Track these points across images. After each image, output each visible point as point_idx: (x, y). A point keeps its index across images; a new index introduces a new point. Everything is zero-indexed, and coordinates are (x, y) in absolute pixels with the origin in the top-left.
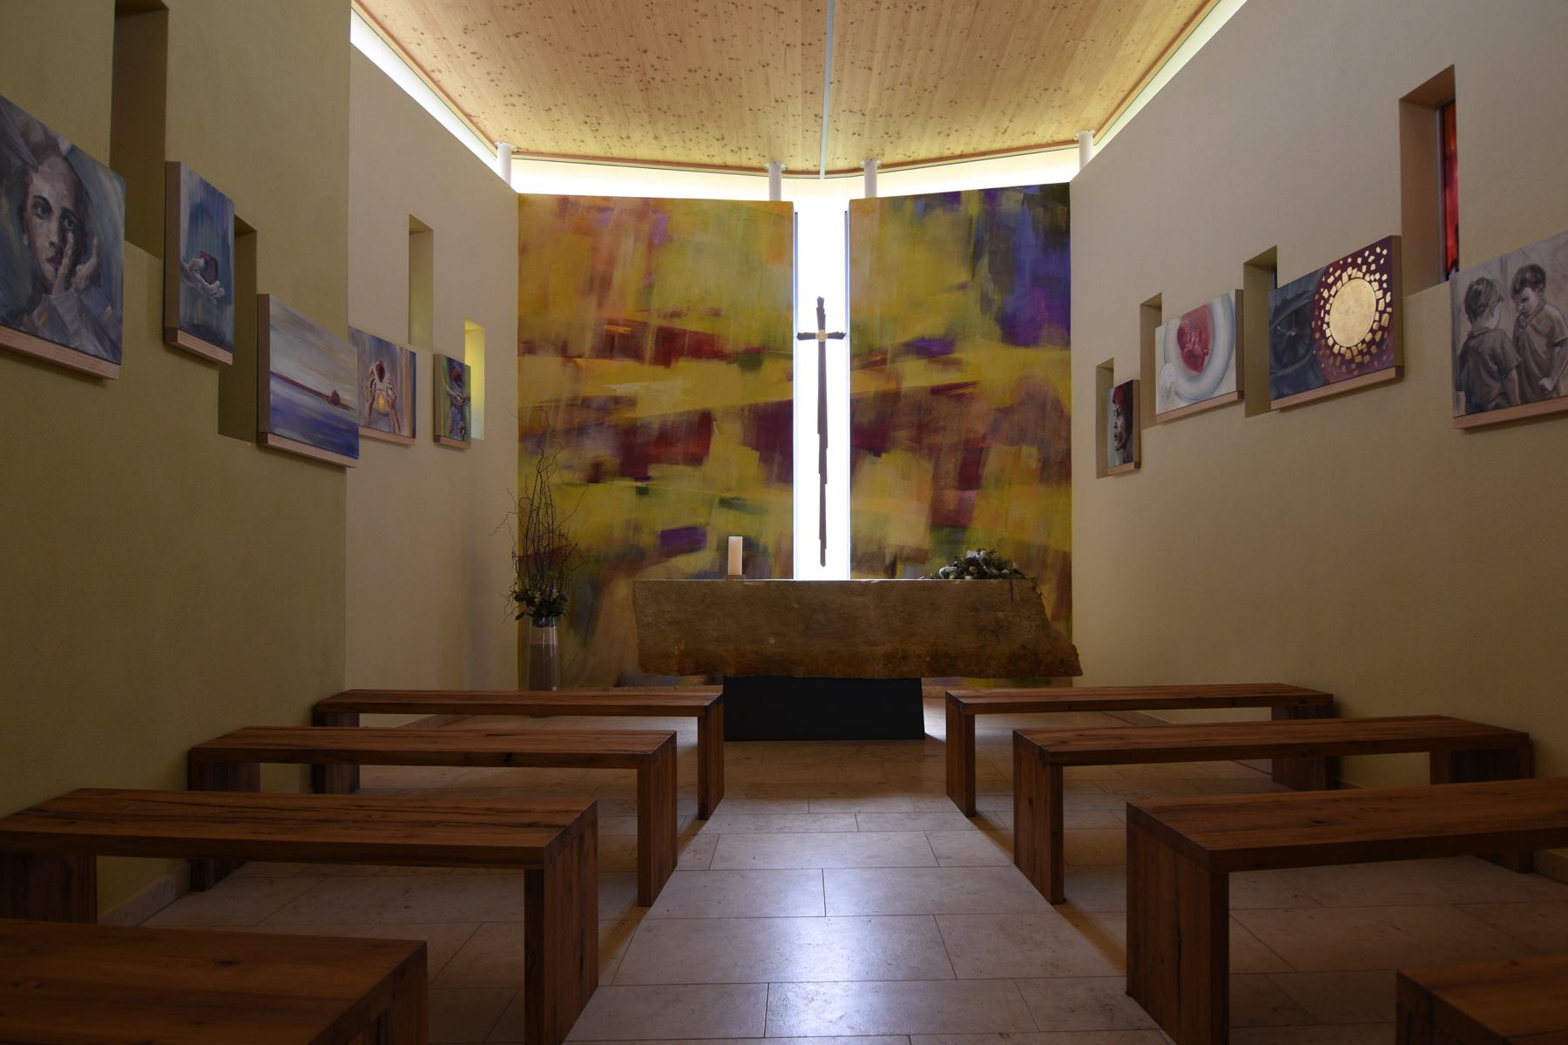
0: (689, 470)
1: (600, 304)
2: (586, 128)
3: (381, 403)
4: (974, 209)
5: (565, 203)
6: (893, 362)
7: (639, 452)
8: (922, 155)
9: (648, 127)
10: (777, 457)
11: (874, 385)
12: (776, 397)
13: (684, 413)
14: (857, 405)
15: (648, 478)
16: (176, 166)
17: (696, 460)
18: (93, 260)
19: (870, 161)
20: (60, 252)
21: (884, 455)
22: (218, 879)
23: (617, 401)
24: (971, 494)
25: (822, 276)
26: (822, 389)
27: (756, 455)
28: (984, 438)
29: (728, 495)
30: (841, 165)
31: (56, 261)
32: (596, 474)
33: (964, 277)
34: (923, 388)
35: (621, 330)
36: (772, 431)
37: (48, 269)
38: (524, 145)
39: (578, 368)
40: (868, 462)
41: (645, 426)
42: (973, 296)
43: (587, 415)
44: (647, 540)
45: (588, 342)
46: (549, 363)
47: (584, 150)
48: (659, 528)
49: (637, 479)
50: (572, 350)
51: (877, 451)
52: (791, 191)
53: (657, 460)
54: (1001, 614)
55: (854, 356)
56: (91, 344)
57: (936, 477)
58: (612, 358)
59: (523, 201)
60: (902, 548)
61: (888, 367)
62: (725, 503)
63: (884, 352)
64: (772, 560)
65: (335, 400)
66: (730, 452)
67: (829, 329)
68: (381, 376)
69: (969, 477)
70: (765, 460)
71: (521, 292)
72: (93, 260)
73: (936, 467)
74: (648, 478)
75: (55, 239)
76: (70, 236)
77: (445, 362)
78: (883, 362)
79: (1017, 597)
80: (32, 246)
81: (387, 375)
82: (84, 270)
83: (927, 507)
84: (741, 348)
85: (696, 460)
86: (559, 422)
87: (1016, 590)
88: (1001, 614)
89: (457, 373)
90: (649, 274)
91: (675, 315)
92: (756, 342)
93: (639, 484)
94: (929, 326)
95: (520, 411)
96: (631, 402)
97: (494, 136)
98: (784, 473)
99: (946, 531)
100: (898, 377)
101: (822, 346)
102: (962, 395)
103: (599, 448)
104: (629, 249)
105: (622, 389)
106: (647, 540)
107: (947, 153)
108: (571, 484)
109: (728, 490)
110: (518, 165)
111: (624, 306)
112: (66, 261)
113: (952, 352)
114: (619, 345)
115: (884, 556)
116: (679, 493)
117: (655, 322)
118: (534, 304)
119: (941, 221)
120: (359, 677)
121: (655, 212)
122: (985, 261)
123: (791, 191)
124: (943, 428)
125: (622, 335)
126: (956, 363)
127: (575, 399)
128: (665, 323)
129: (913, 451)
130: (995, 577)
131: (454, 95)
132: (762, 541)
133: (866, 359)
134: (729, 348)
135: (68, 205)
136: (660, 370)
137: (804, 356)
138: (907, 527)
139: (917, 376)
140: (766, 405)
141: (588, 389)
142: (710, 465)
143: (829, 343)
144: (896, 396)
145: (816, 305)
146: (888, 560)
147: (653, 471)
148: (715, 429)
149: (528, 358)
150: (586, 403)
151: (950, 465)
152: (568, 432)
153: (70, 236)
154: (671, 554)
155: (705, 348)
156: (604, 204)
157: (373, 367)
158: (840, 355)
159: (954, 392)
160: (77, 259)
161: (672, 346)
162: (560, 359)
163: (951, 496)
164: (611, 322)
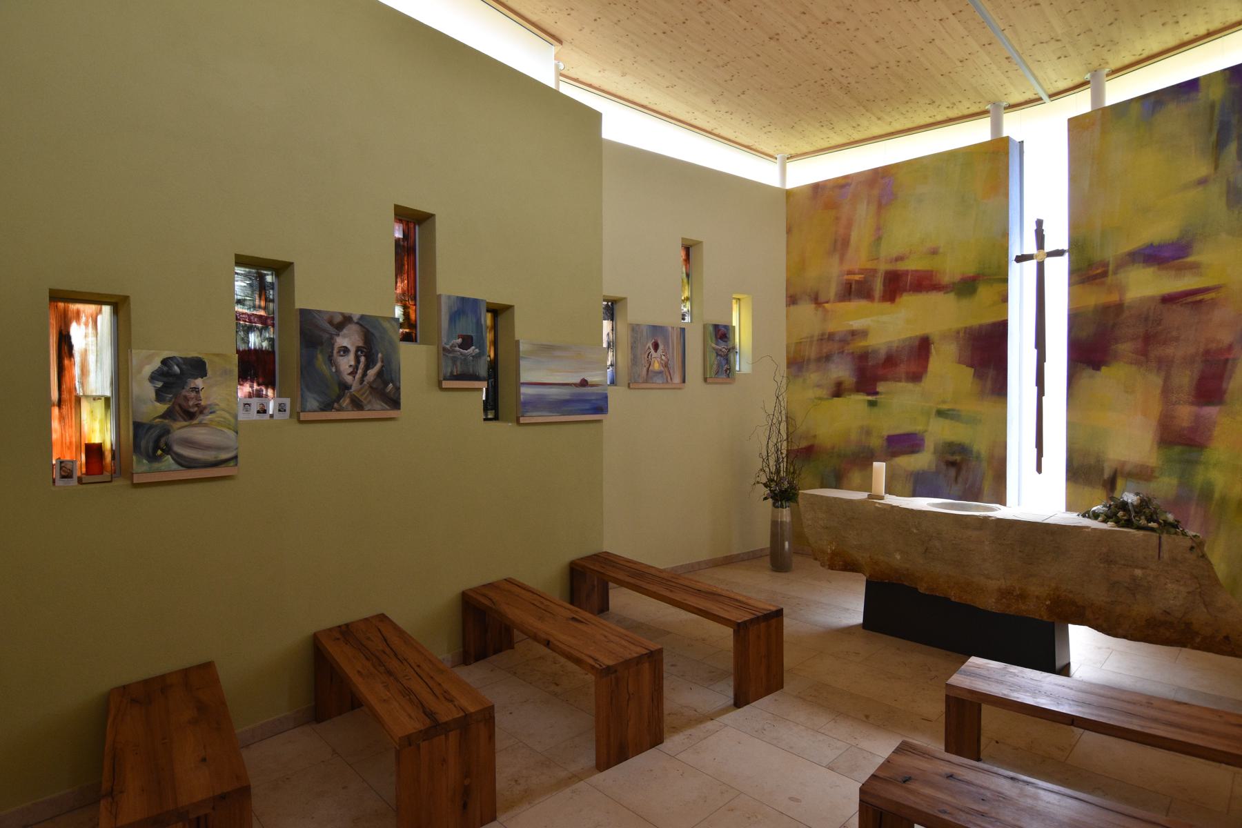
0: (910, 386)
1: (842, 260)
2: (824, 129)
3: (656, 366)
4: (1216, 93)
5: (817, 188)
6: (1115, 273)
7: (869, 373)
8: (1156, 48)
9: (868, 114)
10: (991, 373)
11: (1095, 298)
12: (989, 319)
13: (906, 339)
14: (1075, 319)
15: (876, 393)
16: (440, 296)
17: (916, 377)
18: (379, 365)
19: (1095, 73)
20: (356, 368)
21: (1104, 369)
22: (477, 660)
23: (853, 333)
24: (1211, 411)
25: (1044, 196)
26: (1038, 309)
27: (971, 371)
28: (1230, 348)
29: (944, 407)
30: (1062, 85)
31: (353, 373)
32: (838, 391)
33: (1203, 169)
34: (1152, 298)
35: (857, 277)
36: (987, 351)
37: (349, 379)
38: (793, 152)
39: (826, 311)
40: (1089, 378)
41: (875, 352)
42: (1216, 191)
43: (831, 345)
44: (876, 442)
45: (833, 290)
46: (806, 310)
47: (833, 143)
48: (886, 433)
49: (869, 394)
50: (822, 298)
51: (1096, 365)
52: (1014, 126)
53: (884, 379)
54: (1138, 572)
55: (1073, 272)
56: (378, 404)
57: (1166, 391)
58: (850, 300)
59: (789, 194)
60: (1124, 464)
61: (1110, 279)
62: (940, 413)
63: (1105, 265)
64: (984, 464)
65: (584, 383)
66: (948, 373)
67: (1048, 247)
68: (656, 346)
69: (1210, 390)
70: (979, 375)
71: (788, 259)
72: (379, 365)
73: (1167, 380)
74: (876, 393)
75: (353, 363)
76: (363, 359)
77: (711, 329)
78: (1105, 274)
79: (1166, 555)
80: (338, 371)
81: (661, 347)
82: (372, 373)
83: (1154, 423)
84: (957, 278)
85: (916, 377)
86: (812, 352)
87: (1165, 547)
88: (1138, 572)
89: (722, 333)
90: (878, 229)
91: (900, 259)
92: (971, 270)
93: (870, 398)
94: (1160, 230)
95: (788, 347)
96: (864, 333)
97: (771, 153)
98: (999, 388)
99: (1177, 449)
100: (1122, 289)
101: (1041, 267)
102: (1200, 301)
103: (841, 371)
104: (863, 214)
105: (856, 324)
106: (876, 442)
107: (1186, 38)
108: (820, 399)
109: (944, 402)
110: (792, 166)
111: (859, 258)
112: (360, 371)
113: (1187, 256)
114: (855, 290)
115: (1103, 470)
116: (902, 406)
117: (883, 267)
118: (797, 267)
119: (1174, 118)
120: (619, 540)
121: (883, 178)
122: (1233, 147)
123: (1014, 126)
124: (1177, 339)
125: (857, 282)
126: (1195, 268)
127: (823, 334)
128: (890, 267)
129: (1138, 363)
130: (1139, 528)
131: (732, 138)
132: (976, 448)
133: (1087, 271)
134: (946, 280)
135: (361, 344)
136: (887, 305)
137: (1021, 280)
138: (1131, 440)
139: (1143, 285)
140: (981, 326)
141: (834, 326)
142: (928, 382)
143: (1049, 263)
144: (1119, 307)
145: (1035, 227)
146: (1106, 475)
147: (881, 387)
148: (933, 351)
149: (792, 307)
150: (831, 337)
151: (1185, 379)
152: (819, 360)
153: (363, 359)
154: (894, 454)
155: (925, 283)
156: (843, 182)
157: (650, 345)
158: (1058, 272)
159: (1190, 299)
160: (367, 367)
161: (896, 285)
162: (813, 306)
163: (1185, 413)
164: (850, 273)
